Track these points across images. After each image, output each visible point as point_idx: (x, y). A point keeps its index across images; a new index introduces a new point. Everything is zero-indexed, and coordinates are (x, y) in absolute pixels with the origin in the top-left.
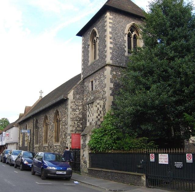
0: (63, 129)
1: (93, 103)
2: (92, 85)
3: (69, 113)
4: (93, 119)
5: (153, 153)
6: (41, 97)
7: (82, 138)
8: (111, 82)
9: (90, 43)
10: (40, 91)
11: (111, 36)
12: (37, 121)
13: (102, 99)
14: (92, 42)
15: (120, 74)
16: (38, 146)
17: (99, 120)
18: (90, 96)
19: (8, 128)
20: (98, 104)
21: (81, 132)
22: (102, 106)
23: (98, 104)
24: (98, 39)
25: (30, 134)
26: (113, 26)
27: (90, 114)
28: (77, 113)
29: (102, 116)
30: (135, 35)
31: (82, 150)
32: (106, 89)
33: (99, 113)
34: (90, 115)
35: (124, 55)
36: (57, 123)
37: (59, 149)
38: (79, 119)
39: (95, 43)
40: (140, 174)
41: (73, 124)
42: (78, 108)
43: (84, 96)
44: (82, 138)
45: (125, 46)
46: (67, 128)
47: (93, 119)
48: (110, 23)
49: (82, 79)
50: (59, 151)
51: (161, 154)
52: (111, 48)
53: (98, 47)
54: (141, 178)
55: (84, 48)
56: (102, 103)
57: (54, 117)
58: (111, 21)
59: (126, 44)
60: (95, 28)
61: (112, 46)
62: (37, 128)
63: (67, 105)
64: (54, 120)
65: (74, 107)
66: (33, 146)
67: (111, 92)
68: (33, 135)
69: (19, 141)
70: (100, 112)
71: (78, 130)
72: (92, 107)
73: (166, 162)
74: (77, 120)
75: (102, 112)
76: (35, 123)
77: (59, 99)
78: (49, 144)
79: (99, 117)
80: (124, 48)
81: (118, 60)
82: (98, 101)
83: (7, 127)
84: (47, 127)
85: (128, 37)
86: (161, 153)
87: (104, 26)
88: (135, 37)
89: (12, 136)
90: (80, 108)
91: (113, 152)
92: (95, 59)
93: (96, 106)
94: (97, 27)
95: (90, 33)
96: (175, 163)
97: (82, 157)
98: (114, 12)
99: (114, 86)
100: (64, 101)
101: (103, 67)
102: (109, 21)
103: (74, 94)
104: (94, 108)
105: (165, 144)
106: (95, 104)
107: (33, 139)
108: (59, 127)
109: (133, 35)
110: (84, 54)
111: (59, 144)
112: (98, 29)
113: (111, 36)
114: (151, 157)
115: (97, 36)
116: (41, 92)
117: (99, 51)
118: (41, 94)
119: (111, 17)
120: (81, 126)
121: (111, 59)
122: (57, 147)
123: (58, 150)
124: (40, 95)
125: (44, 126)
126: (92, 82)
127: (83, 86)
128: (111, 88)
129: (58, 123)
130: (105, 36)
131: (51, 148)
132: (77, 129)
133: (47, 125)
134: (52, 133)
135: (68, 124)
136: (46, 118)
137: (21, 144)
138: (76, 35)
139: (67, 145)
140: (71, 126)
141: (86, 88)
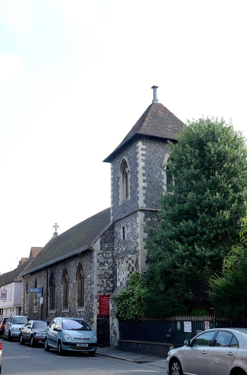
2: (124, 232)
3: (95, 269)
4: (123, 278)
5: (208, 321)
6: (55, 234)
9: (120, 175)
10: (55, 225)
11: (144, 172)
12: (52, 275)
13: (135, 253)
15: (156, 220)
18: (122, 247)
20: (130, 259)
21: (111, 293)
22: (135, 262)
23: (130, 259)
25: (42, 294)
27: (120, 271)
32: (138, 240)
33: (131, 271)
34: (120, 273)
37: (84, 317)
38: (108, 275)
39: (126, 175)
41: (101, 283)
42: (108, 261)
43: (115, 245)
44: (111, 303)
46: (93, 288)
48: (143, 155)
51: (185, 322)
52: (144, 188)
55: (113, 179)
56: (134, 257)
57: (77, 272)
58: (144, 152)
60: (125, 158)
61: (145, 185)
63: (92, 257)
64: (76, 277)
65: (102, 260)
66: (47, 312)
69: (24, 305)
70: (133, 268)
71: (107, 291)
72: (122, 263)
76: (49, 279)
80: (161, 186)
81: (153, 202)
84: (66, 284)
86: (186, 321)
90: (110, 261)
93: (127, 262)
95: (121, 162)
96: (197, 331)
97: (112, 326)
98: (149, 139)
100: (88, 252)
101: (136, 212)
103: (101, 244)
105: (211, 308)
108: (83, 286)
111: (84, 310)
113: (144, 172)
114: (206, 325)
116: (56, 226)
117: (131, 190)
118: (56, 229)
119: (144, 147)
120: (111, 285)
121: (145, 202)
122: (81, 313)
124: (54, 231)
125: (63, 283)
126: (124, 228)
127: (113, 232)
128: (145, 239)
129: (81, 281)
130: (137, 172)
132: (107, 289)
134: (73, 294)
135: (95, 283)
136: (65, 272)
140: (98, 285)
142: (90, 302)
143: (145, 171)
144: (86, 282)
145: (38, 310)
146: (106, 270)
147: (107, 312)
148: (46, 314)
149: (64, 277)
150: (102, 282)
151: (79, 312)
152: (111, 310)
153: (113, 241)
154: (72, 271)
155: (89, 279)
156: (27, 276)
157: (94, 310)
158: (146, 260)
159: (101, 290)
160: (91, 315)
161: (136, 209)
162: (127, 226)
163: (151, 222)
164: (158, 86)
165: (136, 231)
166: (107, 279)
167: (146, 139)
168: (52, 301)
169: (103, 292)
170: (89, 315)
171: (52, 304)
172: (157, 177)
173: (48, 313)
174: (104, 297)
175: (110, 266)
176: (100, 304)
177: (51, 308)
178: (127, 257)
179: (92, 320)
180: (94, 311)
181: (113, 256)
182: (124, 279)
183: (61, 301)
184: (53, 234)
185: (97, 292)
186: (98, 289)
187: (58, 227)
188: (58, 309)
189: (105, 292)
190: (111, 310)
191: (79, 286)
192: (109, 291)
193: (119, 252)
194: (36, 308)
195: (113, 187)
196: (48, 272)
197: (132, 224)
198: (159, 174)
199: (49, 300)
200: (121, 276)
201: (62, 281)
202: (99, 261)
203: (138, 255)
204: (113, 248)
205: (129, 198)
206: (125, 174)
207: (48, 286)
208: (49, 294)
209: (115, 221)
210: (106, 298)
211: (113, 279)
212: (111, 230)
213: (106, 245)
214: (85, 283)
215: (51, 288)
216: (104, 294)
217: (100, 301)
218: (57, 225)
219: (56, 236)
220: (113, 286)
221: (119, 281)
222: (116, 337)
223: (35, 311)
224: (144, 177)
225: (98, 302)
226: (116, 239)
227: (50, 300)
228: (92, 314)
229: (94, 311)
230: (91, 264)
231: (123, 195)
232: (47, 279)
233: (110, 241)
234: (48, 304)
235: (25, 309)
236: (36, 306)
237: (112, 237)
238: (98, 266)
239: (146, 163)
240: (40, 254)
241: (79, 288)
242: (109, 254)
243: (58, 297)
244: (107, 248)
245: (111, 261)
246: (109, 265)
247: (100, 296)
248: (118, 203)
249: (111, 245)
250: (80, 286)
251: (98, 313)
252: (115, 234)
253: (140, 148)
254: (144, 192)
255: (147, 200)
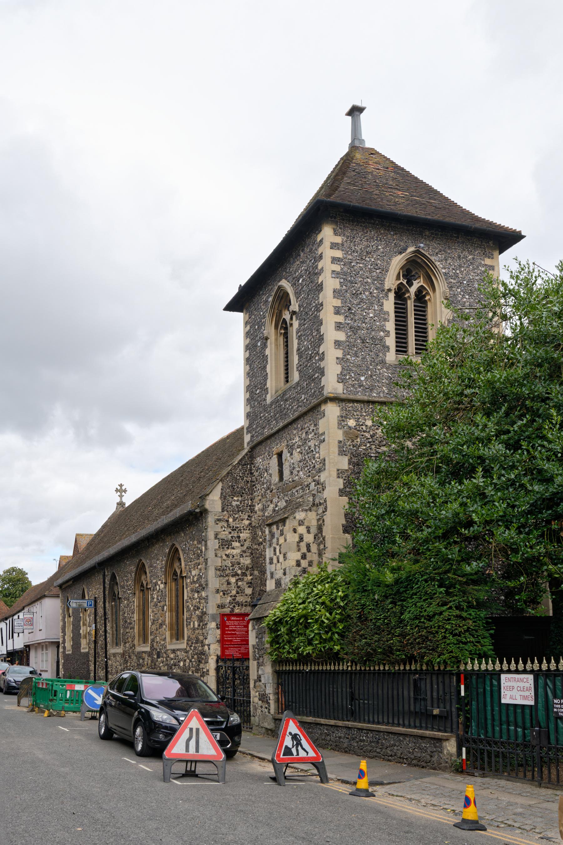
0: (194, 601)
1: (283, 521)
2: (280, 464)
3: (210, 554)
4: (285, 570)
6: (121, 504)
7: (253, 626)
8: (342, 452)
9: (270, 330)
10: (119, 488)
11: (338, 303)
13: (315, 508)
14: (276, 327)
16: (120, 650)
17: (304, 571)
19: (28, 601)
20: (301, 523)
22: (314, 530)
23: (301, 523)
24: (294, 317)
26: (345, 269)
27: (275, 554)
28: (235, 552)
29: (315, 558)
30: (420, 290)
31: (253, 664)
35: (383, 362)
36: (174, 583)
37: (185, 661)
38: (240, 569)
39: (286, 329)
40: (440, 734)
42: (239, 537)
43: (257, 499)
44: (254, 629)
45: (384, 331)
46: (206, 599)
47: (285, 570)
48: (335, 260)
49: (246, 449)
50: (184, 665)
52: (338, 344)
53: (295, 342)
54: (441, 747)
56: (312, 518)
58: (339, 254)
59: (391, 326)
60: (284, 283)
61: (341, 336)
62: (114, 600)
65: (225, 534)
66: (106, 651)
67: (340, 483)
68: (105, 619)
70: (308, 546)
73: (525, 698)
74: (237, 574)
75: (314, 548)
76: (107, 586)
77: (178, 512)
78: (152, 646)
79: (304, 563)
80: (381, 339)
81: (363, 378)
82: (300, 515)
83: (19, 602)
85: (396, 298)
86: (509, 671)
87: (315, 273)
88: (420, 296)
89: (40, 623)
90: (243, 535)
91: (349, 669)
92: (287, 381)
93: (295, 531)
94: (290, 278)
95: (270, 299)
96: (556, 701)
97: (255, 683)
99: (349, 464)
101: (319, 405)
102: (328, 253)
103: (223, 497)
104: (288, 538)
106: (290, 524)
107: (105, 631)
109: (413, 290)
110: (251, 369)
112: (293, 285)
113: (338, 303)
115: (292, 308)
116: (121, 490)
117: (300, 357)
118: (121, 496)
119: (338, 240)
120: (249, 591)
121: (341, 379)
122: (178, 653)
123: (182, 664)
124: (118, 500)
125: (137, 592)
126: (280, 455)
127: (251, 470)
129: (177, 585)
131: (158, 657)
133: (144, 589)
135: (210, 586)
136: (141, 569)
137: (69, 645)
138: (524, 237)
139: (206, 647)
141: (261, 476)
142: (198, 629)
143: (340, 301)
144: (187, 584)
145: (89, 647)
146: (235, 558)
147: (240, 650)
148: (104, 655)
149: (138, 580)
150: (225, 585)
151: (174, 651)
152: (253, 646)
153: (252, 491)
154: (155, 566)
155: (195, 579)
156: (67, 584)
157: (209, 645)
158: (344, 522)
159: (223, 602)
160: (202, 657)
161: (315, 401)
162: (291, 449)
163: (356, 429)
164: (363, 105)
165: (317, 455)
166: (237, 577)
167: (343, 220)
168: (114, 629)
169: (229, 607)
170: (196, 657)
171: (115, 636)
172: (371, 315)
173: (108, 653)
174: (233, 618)
175: (245, 548)
176: (223, 633)
177: (115, 643)
178: (295, 518)
179: (203, 668)
180: (209, 649)
181: (250, 524)
182: (287, 571)
183: (134, 628)
184: (116, 505)
185: (216, 607)
186: (217, 599)
187: (125, 491)
188: (127, 645)
189: (234, 606)
190: (253, 646)
191: (171, 597)
192: (242, 605)
193: (266, 514)
194: (85, 643)
195: (250, 366)
196: (106, 573)
197: (305, 441)
198: (376, 308)
199: (108, 628)
200: (279, 565)
201: (135, 588)
202: (218, 537)
203: (324, 512)
204: (250, 506)
205: (295, 376)
206: (282, 327)
207: (107, 601)
208: (109, 615)
209: (255, 442)
210: (237, 620)
211: (251, 577)
212: (245, 465)
213: (235, 501)
214: (187, 588)
215: (113, 603)
216: (230, 612)
217: (222, 626)
218: (123, 488)
219: (121, 509)
220: (253, 594)
221: (272, 577)
222: (266, 708)
223: (83, 649)
224: (338, 316)
225: (218, 628)
226: (258, 486)
227: (112, 627)
228: (204, 654)
229: (209, 649)
230: (200, 546)
231: (277, 379)
232: (104, 588)
233: (245, 490)
234: (108, 635)
235: (66, 645)
236: (85, 640)
237: (248, 482)
238: (217, 547)
239: (342, 280)
240: (90, 544)
241: (171, 601)
242: (242, 520)
243: (126, 622)
244: (238, 506)
245: (248, 535)
246: (242, 546)
247: (223, 615)
248: (265, 400)
249: (248, 500)
250: (174, 595)
251: (219, 654)
252: (256, 474)
253: (327, 244)
254: (339, 353)
255: (345, 375)
